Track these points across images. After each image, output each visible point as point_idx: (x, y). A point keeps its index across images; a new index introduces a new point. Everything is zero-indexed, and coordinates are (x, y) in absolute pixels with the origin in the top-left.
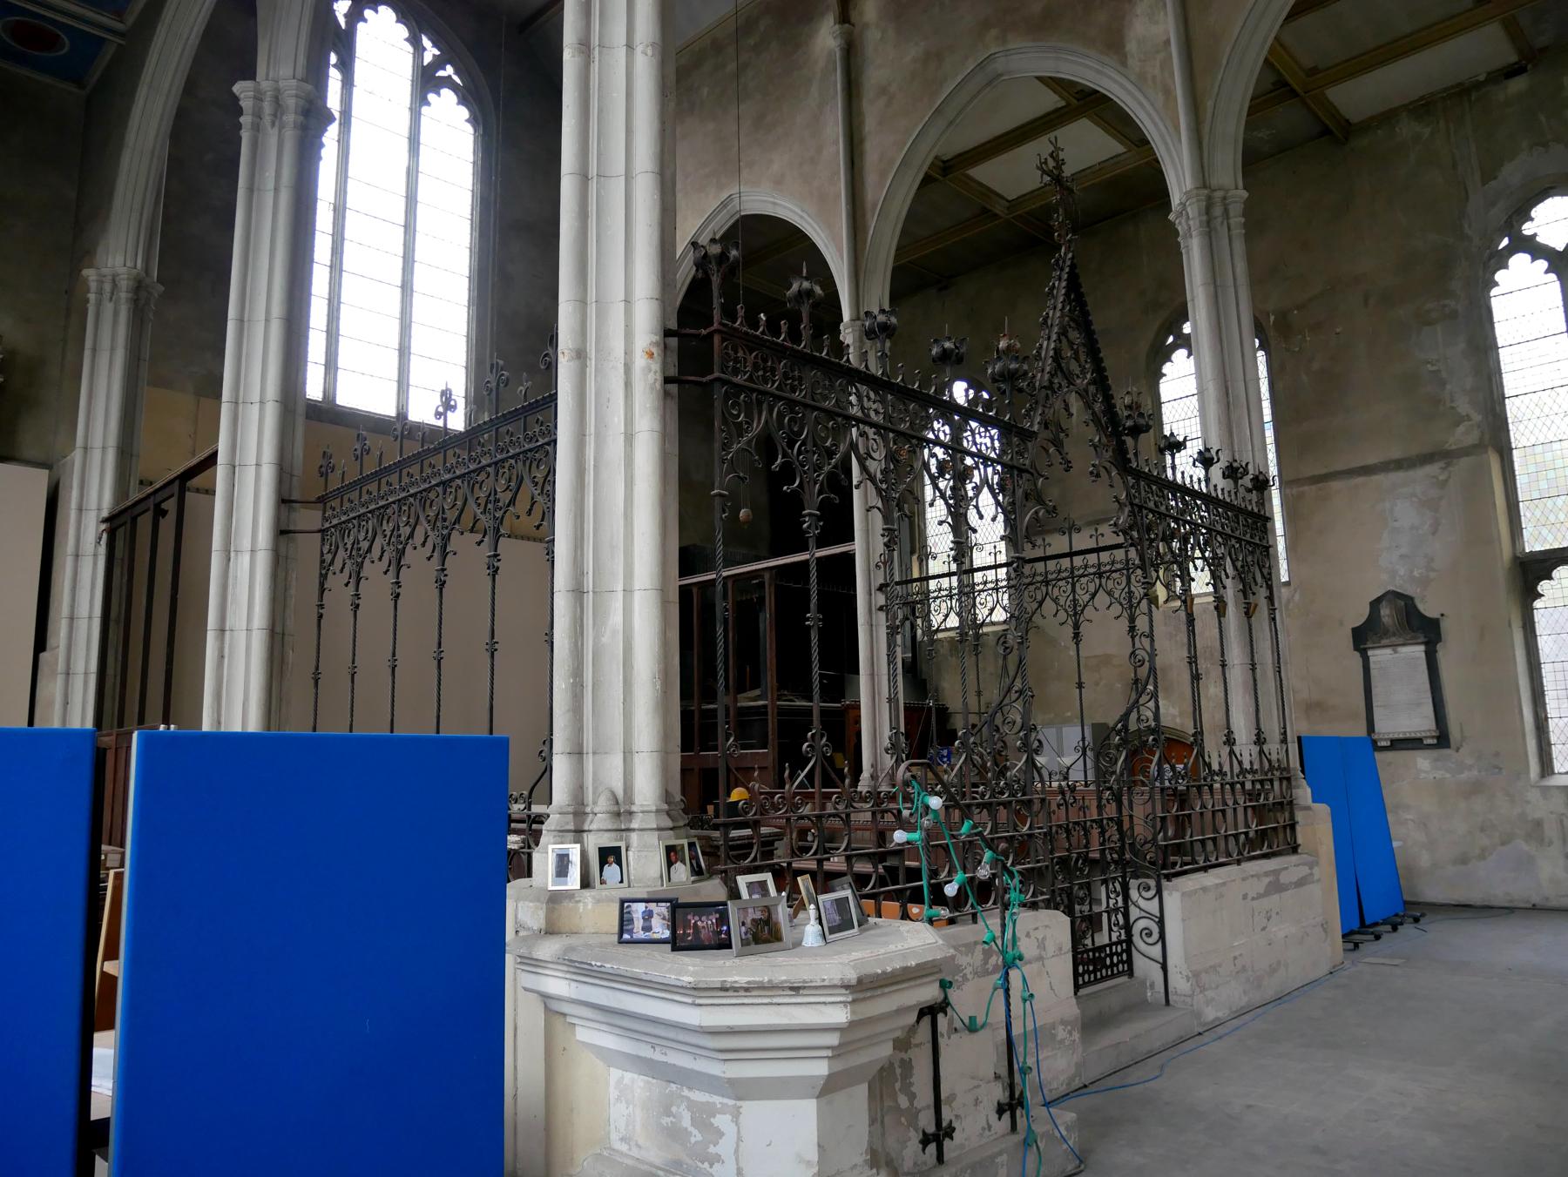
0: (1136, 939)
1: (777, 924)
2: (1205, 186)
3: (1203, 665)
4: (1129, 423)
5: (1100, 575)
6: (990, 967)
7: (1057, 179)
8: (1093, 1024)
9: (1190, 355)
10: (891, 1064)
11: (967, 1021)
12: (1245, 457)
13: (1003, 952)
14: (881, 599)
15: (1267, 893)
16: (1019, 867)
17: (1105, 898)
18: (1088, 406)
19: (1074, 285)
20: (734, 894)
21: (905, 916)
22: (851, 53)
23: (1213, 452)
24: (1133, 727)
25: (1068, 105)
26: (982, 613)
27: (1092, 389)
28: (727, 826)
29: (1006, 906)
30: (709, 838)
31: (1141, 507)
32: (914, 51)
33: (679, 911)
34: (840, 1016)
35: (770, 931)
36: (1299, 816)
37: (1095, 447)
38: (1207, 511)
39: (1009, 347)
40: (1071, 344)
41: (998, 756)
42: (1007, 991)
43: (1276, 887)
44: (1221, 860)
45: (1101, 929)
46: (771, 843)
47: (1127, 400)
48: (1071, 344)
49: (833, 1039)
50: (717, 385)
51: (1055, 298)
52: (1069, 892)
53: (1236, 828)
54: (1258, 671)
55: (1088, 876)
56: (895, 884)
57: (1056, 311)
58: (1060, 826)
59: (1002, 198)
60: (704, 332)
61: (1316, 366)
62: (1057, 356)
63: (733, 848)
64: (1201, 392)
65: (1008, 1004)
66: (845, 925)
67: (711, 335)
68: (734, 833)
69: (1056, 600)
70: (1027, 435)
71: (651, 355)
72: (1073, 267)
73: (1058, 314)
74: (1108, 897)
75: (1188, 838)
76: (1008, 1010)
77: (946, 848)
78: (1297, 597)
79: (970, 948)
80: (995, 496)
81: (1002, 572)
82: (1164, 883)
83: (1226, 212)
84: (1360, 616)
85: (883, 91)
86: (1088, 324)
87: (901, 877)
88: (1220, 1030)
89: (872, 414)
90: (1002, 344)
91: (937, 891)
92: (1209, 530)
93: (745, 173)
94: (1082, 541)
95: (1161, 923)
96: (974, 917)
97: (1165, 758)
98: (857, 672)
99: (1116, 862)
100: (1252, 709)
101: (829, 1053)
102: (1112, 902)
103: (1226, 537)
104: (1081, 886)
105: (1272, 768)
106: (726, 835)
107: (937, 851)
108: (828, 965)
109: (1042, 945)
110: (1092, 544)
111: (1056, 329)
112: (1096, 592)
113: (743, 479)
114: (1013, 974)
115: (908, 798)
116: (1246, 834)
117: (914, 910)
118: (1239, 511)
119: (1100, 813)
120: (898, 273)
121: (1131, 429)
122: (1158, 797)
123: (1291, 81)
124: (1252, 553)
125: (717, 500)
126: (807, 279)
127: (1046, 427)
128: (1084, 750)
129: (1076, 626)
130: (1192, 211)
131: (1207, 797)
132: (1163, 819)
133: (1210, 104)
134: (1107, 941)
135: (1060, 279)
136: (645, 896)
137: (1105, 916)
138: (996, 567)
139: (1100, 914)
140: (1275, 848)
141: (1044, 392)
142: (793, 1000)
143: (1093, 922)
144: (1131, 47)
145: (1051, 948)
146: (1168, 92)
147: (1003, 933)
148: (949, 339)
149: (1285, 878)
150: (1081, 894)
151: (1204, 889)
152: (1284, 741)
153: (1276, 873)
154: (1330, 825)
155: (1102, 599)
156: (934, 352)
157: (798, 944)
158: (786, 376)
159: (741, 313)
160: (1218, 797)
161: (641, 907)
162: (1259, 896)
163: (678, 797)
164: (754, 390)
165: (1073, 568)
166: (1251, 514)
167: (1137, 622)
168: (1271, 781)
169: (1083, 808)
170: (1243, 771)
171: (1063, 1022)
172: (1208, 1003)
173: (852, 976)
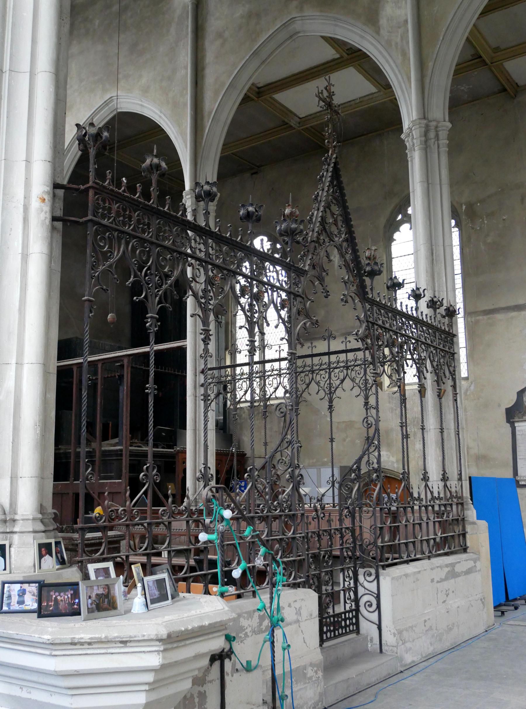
0: (362, 609)
1: (114, 597)
2: (424, 118)
3: (411, 429)
4: (368, 269)
5: (347, 368)
6: (263, 627)
7: (329, 105)
8: (331, 666)
9: (411, 229)
10: (192, 696)
11: (245, 664)
12: (442, 295)
13: (271, 617)
14: (201, 379)
15: (446, 579)
16: (285, 560)
17: (343, 581)
18: (342, 255)
19: (336, 174)
20: (86, 577)
21: (207, 592)
24: (364, 469)
25: (342, 57)
26: (269, 390)
27: (345, 244)
28: (83, 530)
29: (274, 585)
30: (71, 539)
31: (373, 324)
32: (240, 11)
33: (45, 590)
34: (154, 660)
35: (109, 602)
36: (468, 528)
37: (345, 283)
38: (416, 328)
39: (291, 213)
40: (333, 214)
41: (273, 485)
42: (273, 643)
43: (453, 574)
44: (418, 556)
45: (339, 602)
46: (118, 542)
47: (367, 254)
48: (333, 214)
49: (150, 678)
50: (90, 224)
52: (318, 577)
53: (428, 536)
54: (445, 434)
55: (332, 566)
56: (200, 571)
57: (323, 192)
58: (314, 533)
59: (295, 115)
60: (82, 187)
61: (489, 240)
62: (323, 222)
63: (87, 545)
64: (416, 252)
65: (273, 652)
66: (163, 597)
67: (87, 190)
68: (89, 535)
69: (318, 383)
70: (301, 272)
71: (43, 200)
72: (336, 164)
73: (325, 194)
74: (344, 580)
75: (397, 542)
76: (273, 656)
77: (234, 545)
78: (472, 388)
79: (250, 614)
80: (278, 311)
81: (284, 364)
82: (381, 571)
83: (437, 137)
84: (510, 400)
85: (220, 35)
86: (344, 202)
87: (205, 565)
88: (415, 669)
89: (198, 251)
90: (287, 211)
91: (228, 574)
92: (417, 341)
93: (122, 83)
94: (336, 345)
95: (378, 597)
96: (254, 593)
97: (383, 489)
98: (185, 428)
99: (350, 558)
100: (441, 458)
101: (147, 687)
102: (347, 584)
103: (428, 346)
104: (327, 573)
105: (452, 496)
106: (83, 536)
107: (229, 549)
108: (148, 625)
109: (298, 612)
110: (342, 347)
111: (323, 204)
113: (105, 291)
114: (278, 633)
115: (210, 513)
116: (434, 539)
117: (215, 589)
119: (341, 524)
120: (224, 161)
121: (368, 273)
122: (378, 515)
123: (483, 55)
124: (444, 357)
125: (87, 304)
126: (156, 156)
127: (314, 268)
128: (333, 483)
129: (331, 401)
130: (416, 133)
131: (410, 515)
132: (381, 528)
133: (431, 64)
134: (342, 610)
135: (327, 171)
136: (21, 579)
137: (342, 592)
138: (280, 360)
139: (339, 592)
140: (453, 549)
141: (313, 244)
142: (122, 650)
143: (334, 597)
144: (383, 22)
145: (305, 613)
146: (404, 54)
147: (271, 603)
148: (252, 205)
149: (458, 568)
150: (327, 578)
151: (406, 575)
152: (460, 479)
153: (453, 565)
154: (487, 534)
155: (348, 383)
156: (241, 213)
157: (128, 611)
158: (139, 222)
159: (109, 176)
160: (417, 515)
161: (17, 587)
162: (442, 581)
163: (50, 510)
164: (116, 230)
165: (330, 363)
166: (444, 332)
167: (370, 400)
168: (451, 505)
169: (329, 521)
170: (433, 498)
171: (311, 665)
172: (407, 651)
173: (163, 633)
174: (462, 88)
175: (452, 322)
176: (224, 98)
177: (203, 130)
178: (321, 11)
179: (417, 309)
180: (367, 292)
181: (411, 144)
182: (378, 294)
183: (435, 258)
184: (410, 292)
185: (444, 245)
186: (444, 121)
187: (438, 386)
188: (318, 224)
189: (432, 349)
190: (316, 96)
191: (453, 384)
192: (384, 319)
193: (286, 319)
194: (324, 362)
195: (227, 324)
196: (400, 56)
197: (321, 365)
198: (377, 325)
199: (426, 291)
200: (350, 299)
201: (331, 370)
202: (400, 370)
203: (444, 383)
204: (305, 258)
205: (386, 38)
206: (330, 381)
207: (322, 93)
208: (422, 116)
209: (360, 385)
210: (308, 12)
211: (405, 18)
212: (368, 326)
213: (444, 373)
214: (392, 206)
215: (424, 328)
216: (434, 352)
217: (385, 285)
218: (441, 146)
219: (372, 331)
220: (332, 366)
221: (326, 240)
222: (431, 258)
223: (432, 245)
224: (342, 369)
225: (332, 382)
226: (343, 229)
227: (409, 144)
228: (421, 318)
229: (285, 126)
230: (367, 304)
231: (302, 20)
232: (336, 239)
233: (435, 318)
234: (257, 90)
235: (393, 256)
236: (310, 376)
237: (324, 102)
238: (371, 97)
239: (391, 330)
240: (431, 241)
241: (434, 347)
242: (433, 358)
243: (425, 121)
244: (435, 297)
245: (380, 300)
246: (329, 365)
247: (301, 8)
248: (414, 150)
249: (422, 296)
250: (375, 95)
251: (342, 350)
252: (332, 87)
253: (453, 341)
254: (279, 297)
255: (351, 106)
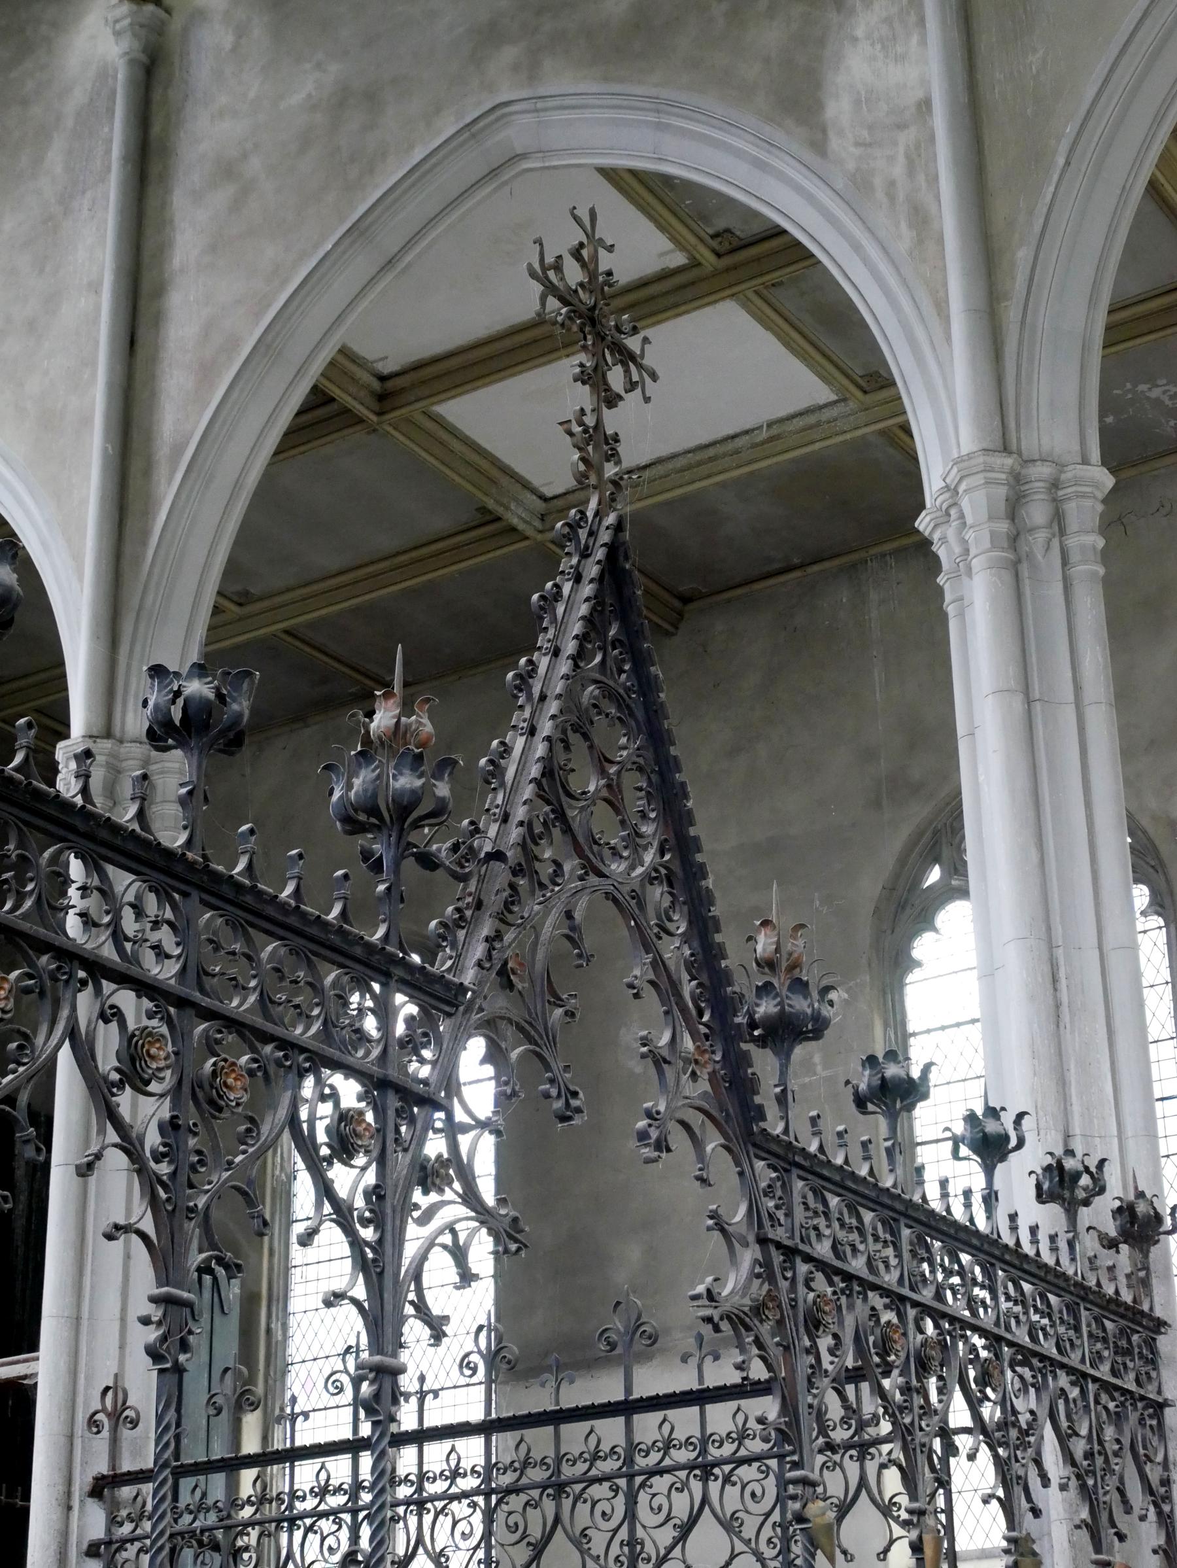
2: (1006, 449)
4: (766, 1008)
12: (1088, 1151)
14: (93, 1522)
22: (154, 74)
23: (1008, 1119)
25: (695, 264)
27: (658, 894)
31: (790, 1253)
32: (308, 85)
47: (764, 944)
51: (561, 627)
59: (526, 485)
62: (552, 783)
72: (613, 549)
83: (1058, 519)
85: (227, 170)
111: (553, 707)
112: (693, 1520)
118: (1079, 1294)
124: (1118, 1419)
127: (505, 976)
130: (975, 504)
133: (1023, 255)
135: (578, 579)
144: (838, 109)
146: (921, 220)
165: (632, 1447)
166: (1113, 1305)
174: (1155, 393)
175: (1146, 1268)
176: (235, 395)
177: (148, 513)
178: (606, 79)
179: (990, 1199)
180: (760, 1109)
181: (957, 550)
182: (814, 1121)
183: (1065, 1000)
184: (959, 1128)
185: (1100, 948)
186: (1085, 461)
187: (1098, 1549)
188: (528, 791)
189: (1063, 1380)
190: (533, 274)
191: (1162, 1541)
192: (842, 1235)
193: (359, 1202)
194: (605, 1447)
195: (250, 1301)
196: (903, 226)
197: (595, 1457)
198: (808, 1259)
199: (1026, 1122)
200: (678, 1139)
201: (639, 1480)
202: (927, 1473)
203: (1121, 1537)
204: (461, 934)
205: (851, 166)
206: (632, 1531)
207: (558, 266)
208: (999, 444)
209: (763, 1547)
210: (561, 80)
211: (920, 94)
212: (767, 1264)
213: (1121, 1491)
214: (904, 833)
215: (1026, 1287)
216: (1074, 1393)
217: (850, 1090)
218: (1075, 557)
219: (784, 1285)
220: (641, 1462)
221: (567, 868)
222: (1051, 1001)
223: (1051, 947)
224: (682, 1474)
225: (640, 1533)
226: (647, 829)
227: (950, 551)
228: (1008, 1239)
229: (489, 523)
230: (760, 1165)
231: (537, 111)
232: (617, 868)
233: (1071, 1244)
234: (376, 385)
235: (911, 1028)
236: (549, 1506)
237: (565, 302)
238: (811, 419)
239: (875, 1287)
240: (1049, 929)
241: (1070, 1370)
242: (1069, 1417)
243: (1009, 461)
244: (1070, 1153)
245: (821, 1148)
246: (629, 1461)
247: (530, 69)
248: (969, 572)
249: (1013, 1142)
250: (826, 415)
251: (683, 1393)
252: (602, 252)
253: (1153, 1350)
254: (323, 1098)
255: (737, 452)
